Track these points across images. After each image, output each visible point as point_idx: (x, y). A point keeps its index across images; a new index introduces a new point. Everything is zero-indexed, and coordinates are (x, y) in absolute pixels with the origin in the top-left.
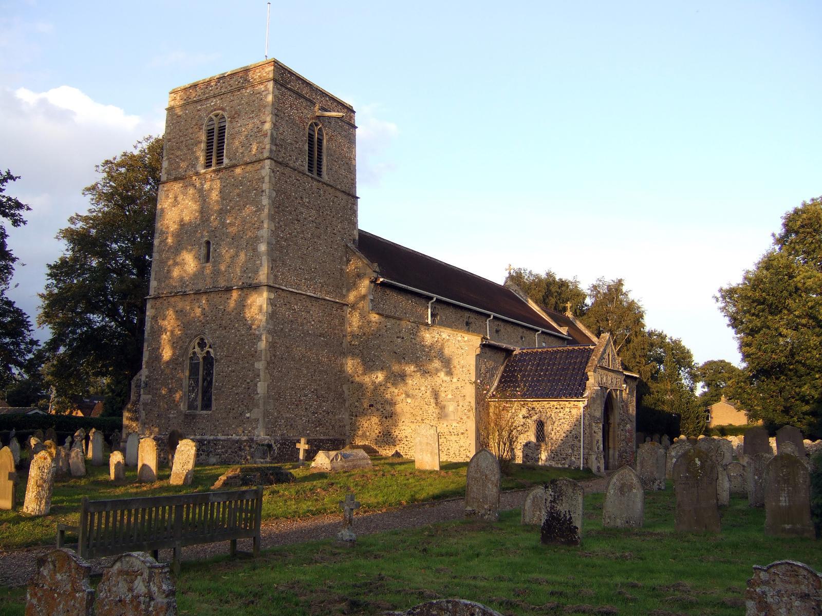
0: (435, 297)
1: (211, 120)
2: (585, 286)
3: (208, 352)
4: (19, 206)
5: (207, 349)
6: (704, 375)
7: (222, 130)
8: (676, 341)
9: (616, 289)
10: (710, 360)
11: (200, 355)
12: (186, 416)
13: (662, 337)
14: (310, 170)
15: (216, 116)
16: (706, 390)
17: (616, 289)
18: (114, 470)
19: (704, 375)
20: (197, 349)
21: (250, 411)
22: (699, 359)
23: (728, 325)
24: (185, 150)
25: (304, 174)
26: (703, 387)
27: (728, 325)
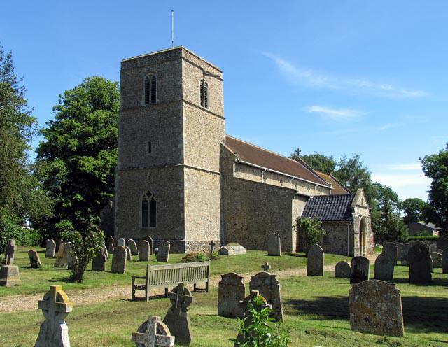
0: (266, 169)
1: (147, 78)
2: (337, 159)
3: (153, 198)
4: (36, 118)
5: (152, 196)
6: (405, 206)
7: (154, 84)
8: (388, 188)
9: (353, 163)
10: (413, 197)
11: (149, 200)
12: (142, 229)
13: (379, 186)
14: (202, 105)
15: (150, 76)
16: (406, 215)
17: (353, 163)
18: (248, 175)
19: (405, 206)
20: (146, 197)
21: (177, 227)
22: (402, 198)
23: (331, 158)
24: (133, 94)
25: (199, 108)
26: (404, 213)
27: (331, 158)
